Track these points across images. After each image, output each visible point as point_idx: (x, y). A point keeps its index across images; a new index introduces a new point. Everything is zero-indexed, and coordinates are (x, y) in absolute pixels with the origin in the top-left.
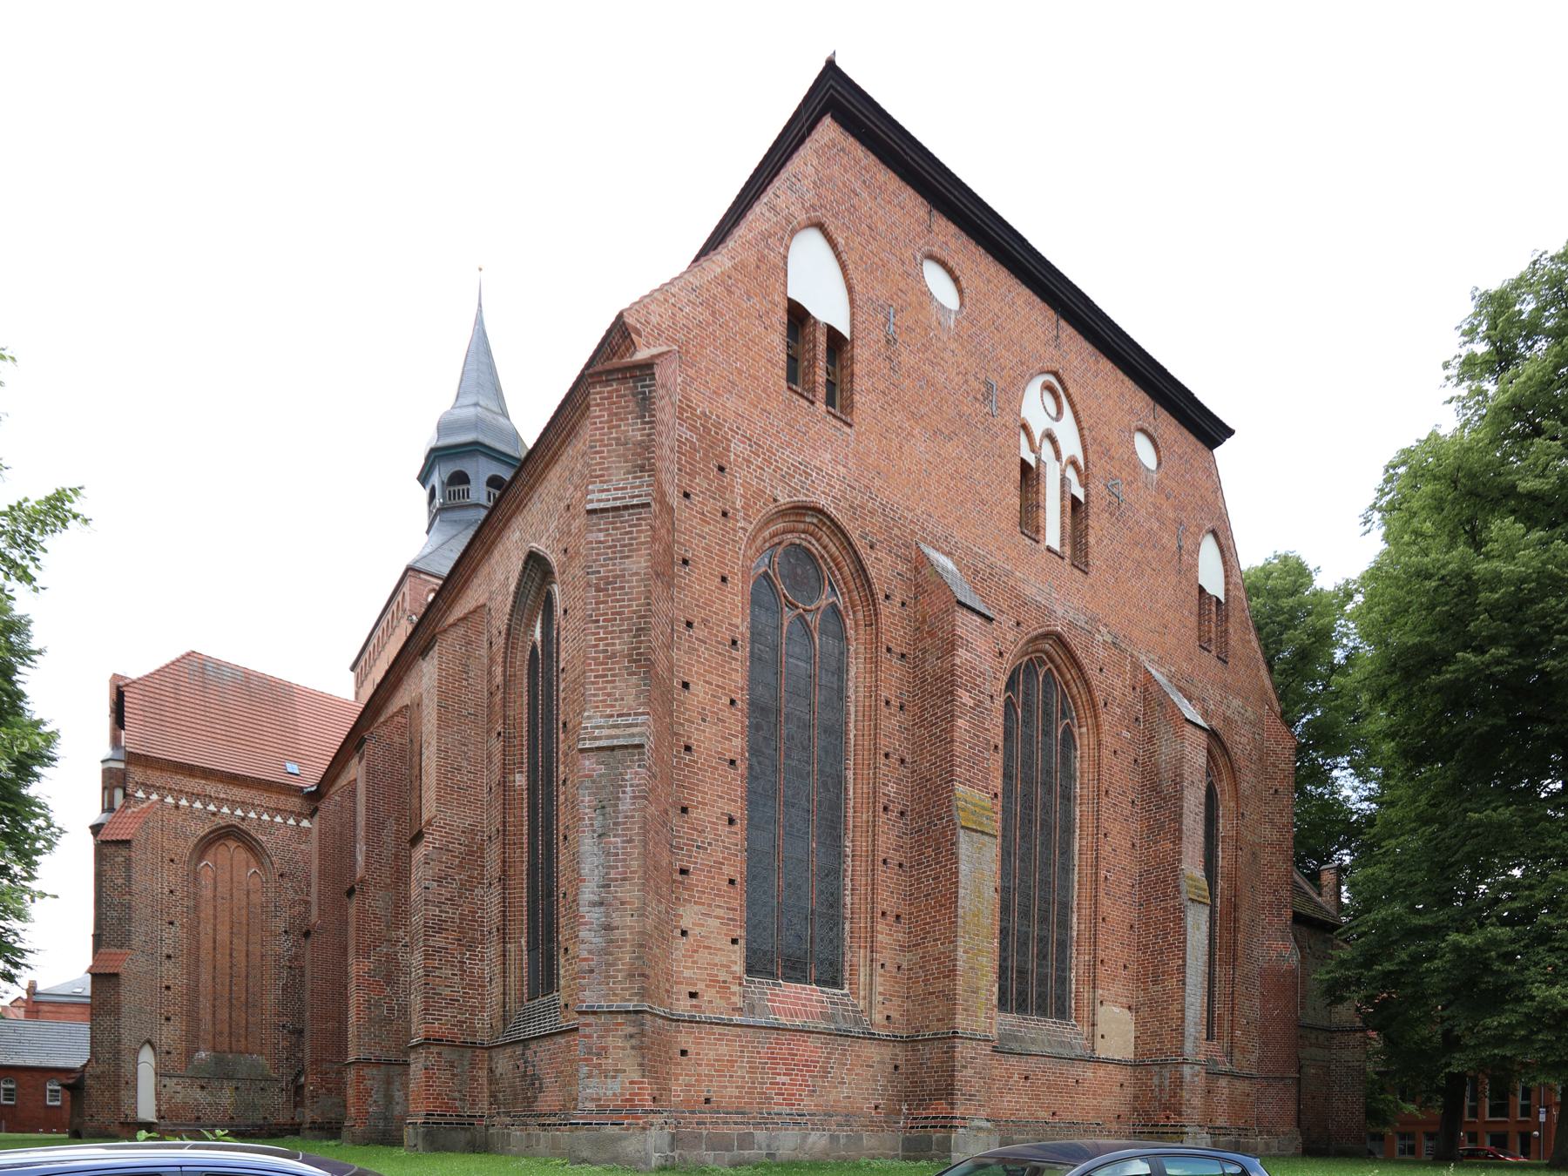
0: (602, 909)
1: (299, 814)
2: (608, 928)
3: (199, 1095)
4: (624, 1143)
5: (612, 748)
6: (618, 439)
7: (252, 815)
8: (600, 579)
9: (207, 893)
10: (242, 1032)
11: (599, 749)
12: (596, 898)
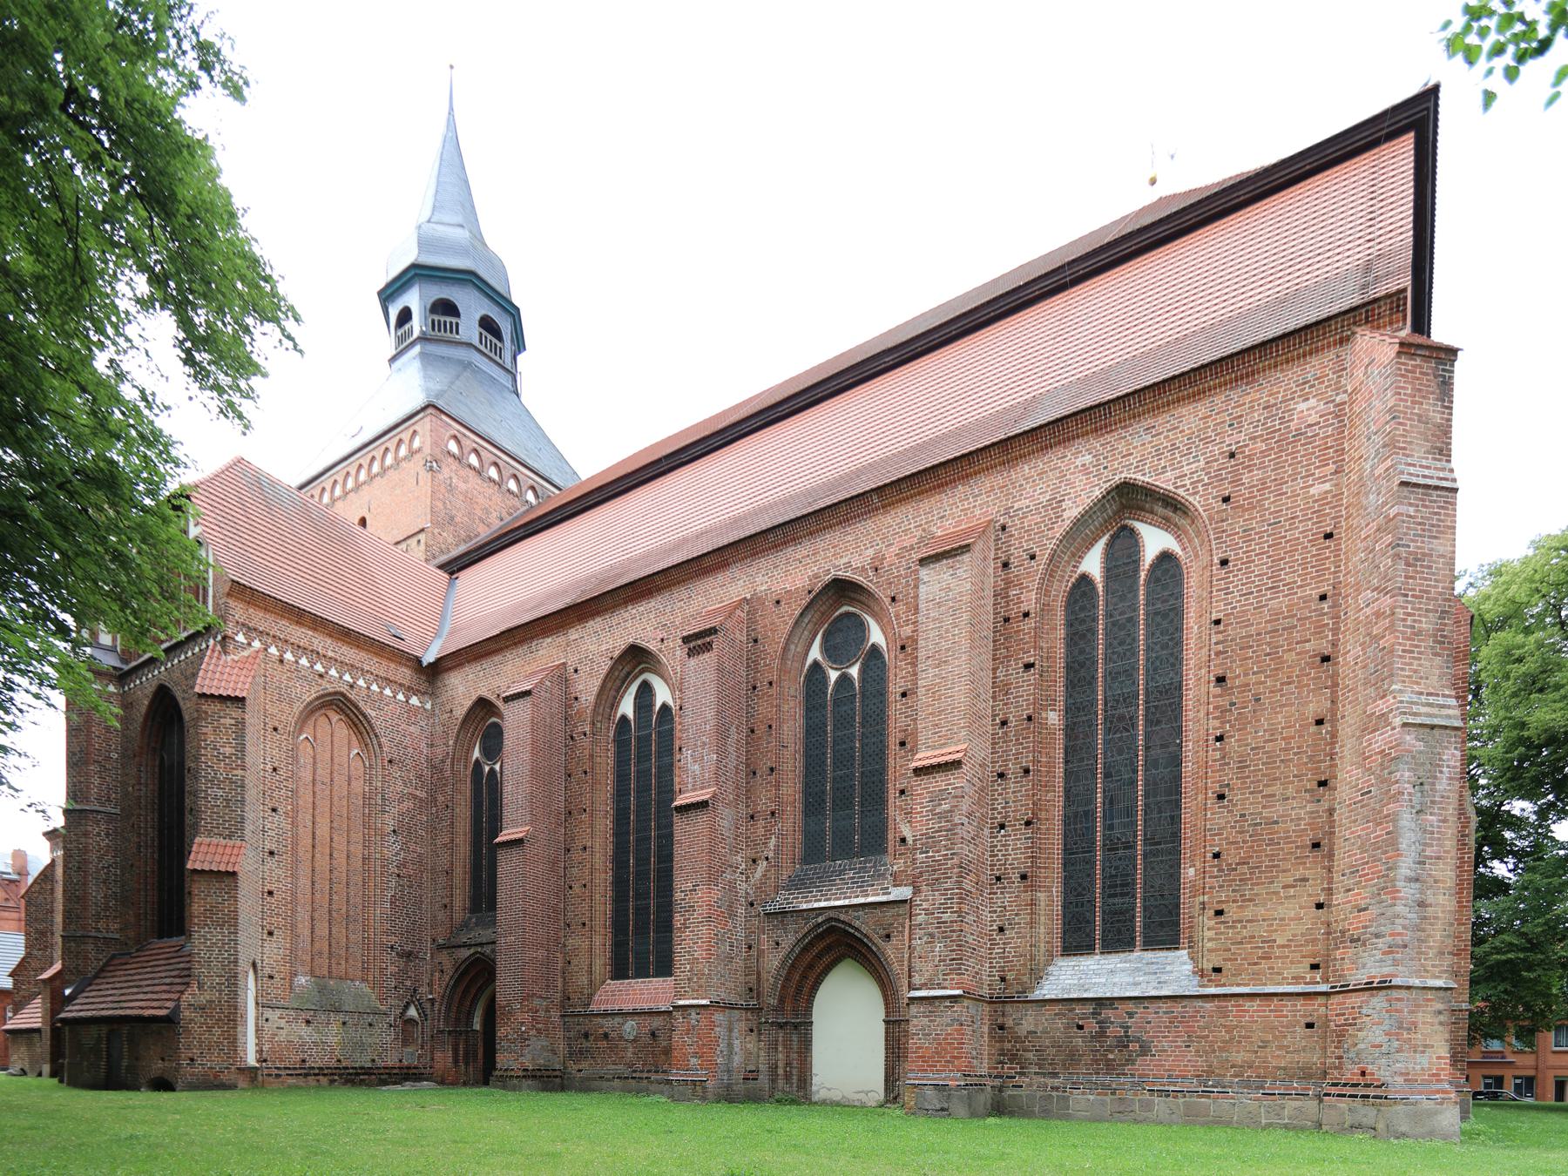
0: (1418, 885)
1: (409, 689)
2: (1422, 904)
3: (305, 1031)
4: (1440, 1117)
5: (1433, 727)
6: (1420, 416)
7: (361, 682)
8: (1410, 553)
9: (306, 775)
10: (343, 952)
11: (1421, 725)
12: (1413, 874)
